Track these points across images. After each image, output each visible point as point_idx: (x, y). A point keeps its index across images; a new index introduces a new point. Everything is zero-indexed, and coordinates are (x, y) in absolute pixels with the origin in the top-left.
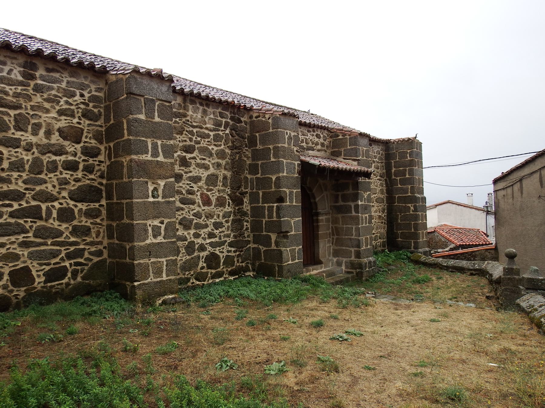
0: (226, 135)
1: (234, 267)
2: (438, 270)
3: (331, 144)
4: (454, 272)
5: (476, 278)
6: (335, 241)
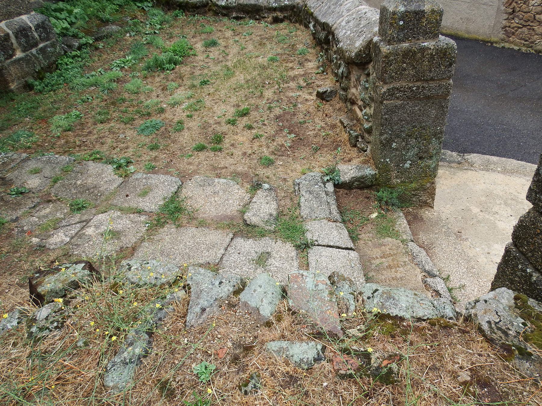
2: (210, 17)
4: (241, 18)
5: (284, 28)
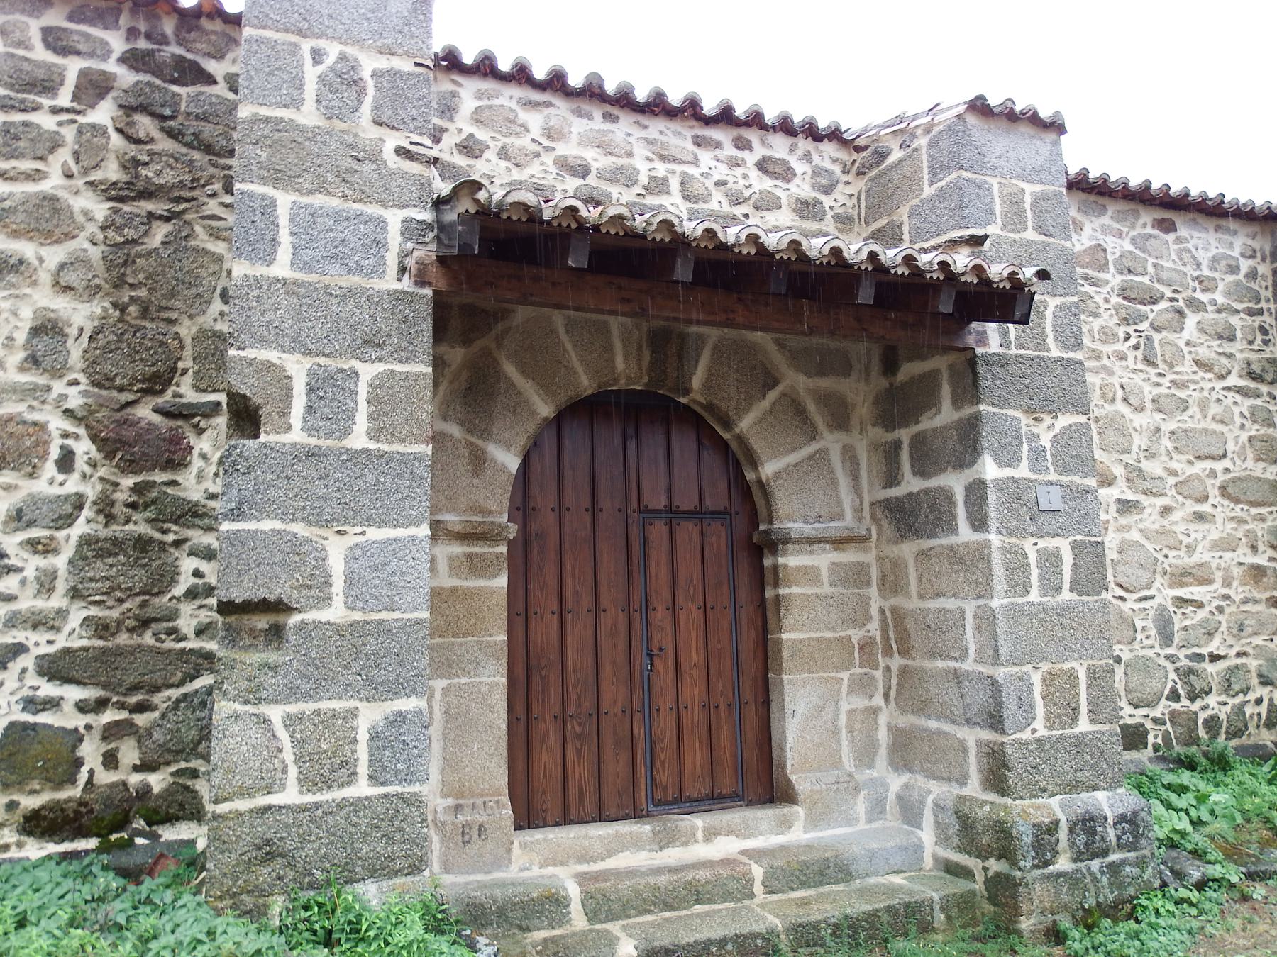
0: (80, 132)
1: (75, 792)
3: (863, 204)
6: (894, 682)
